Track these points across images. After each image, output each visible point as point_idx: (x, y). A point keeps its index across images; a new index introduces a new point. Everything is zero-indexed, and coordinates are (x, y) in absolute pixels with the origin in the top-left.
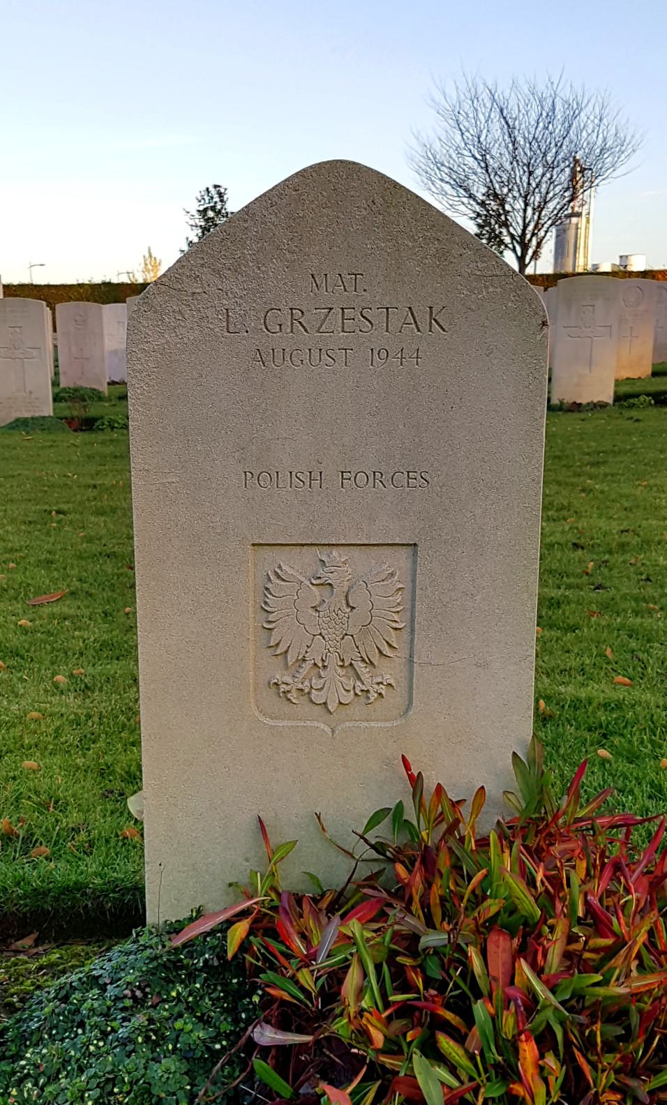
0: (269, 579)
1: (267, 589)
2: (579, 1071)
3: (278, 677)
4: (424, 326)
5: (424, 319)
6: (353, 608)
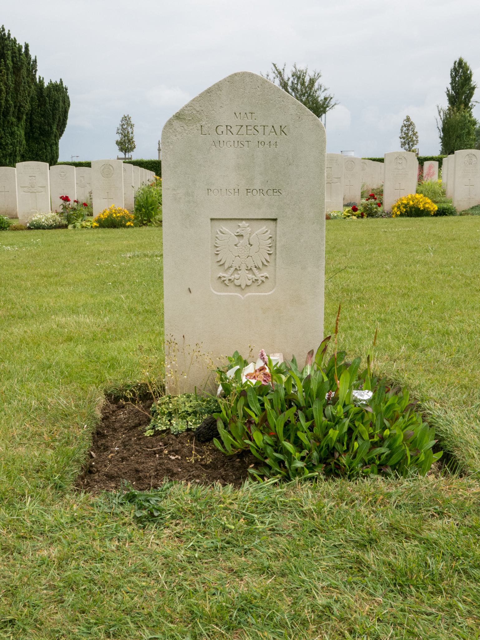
0: (217, 234)
1: (217, 237)
2: (281, 452)
3: (221, 274)
4: (278, 133)
5: (278, 130)
6: (251, 245)
